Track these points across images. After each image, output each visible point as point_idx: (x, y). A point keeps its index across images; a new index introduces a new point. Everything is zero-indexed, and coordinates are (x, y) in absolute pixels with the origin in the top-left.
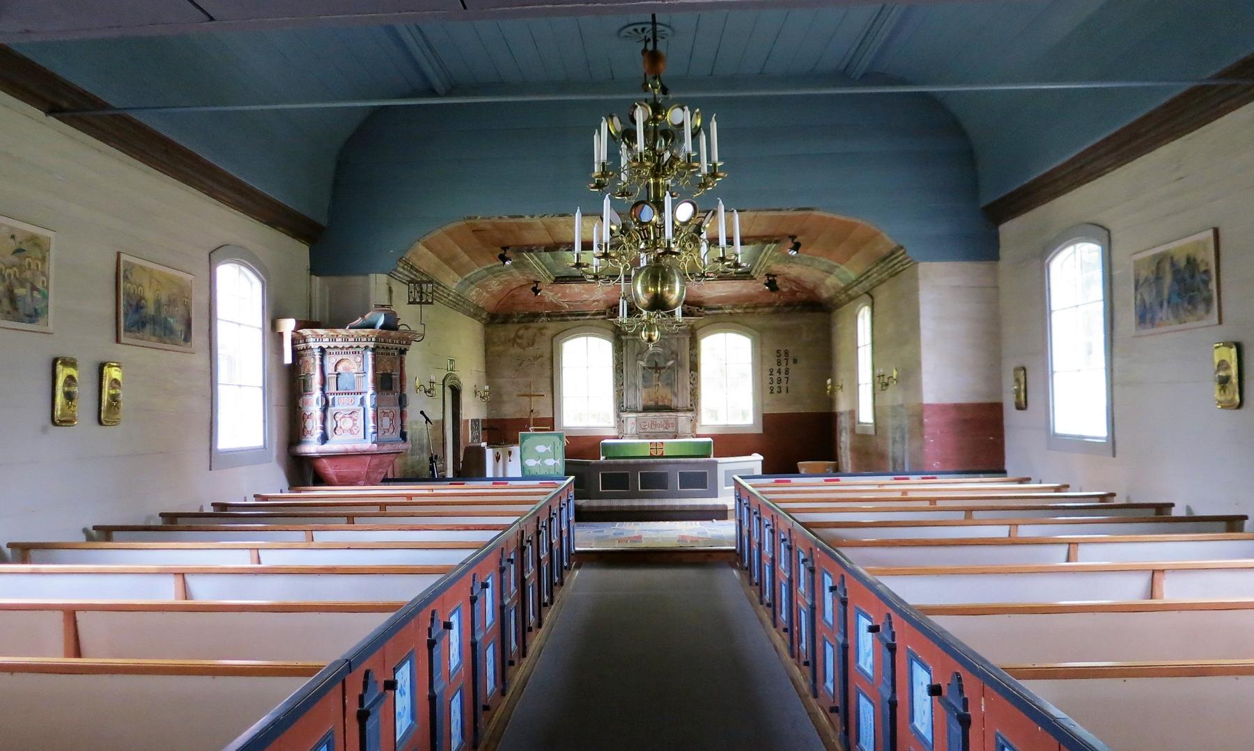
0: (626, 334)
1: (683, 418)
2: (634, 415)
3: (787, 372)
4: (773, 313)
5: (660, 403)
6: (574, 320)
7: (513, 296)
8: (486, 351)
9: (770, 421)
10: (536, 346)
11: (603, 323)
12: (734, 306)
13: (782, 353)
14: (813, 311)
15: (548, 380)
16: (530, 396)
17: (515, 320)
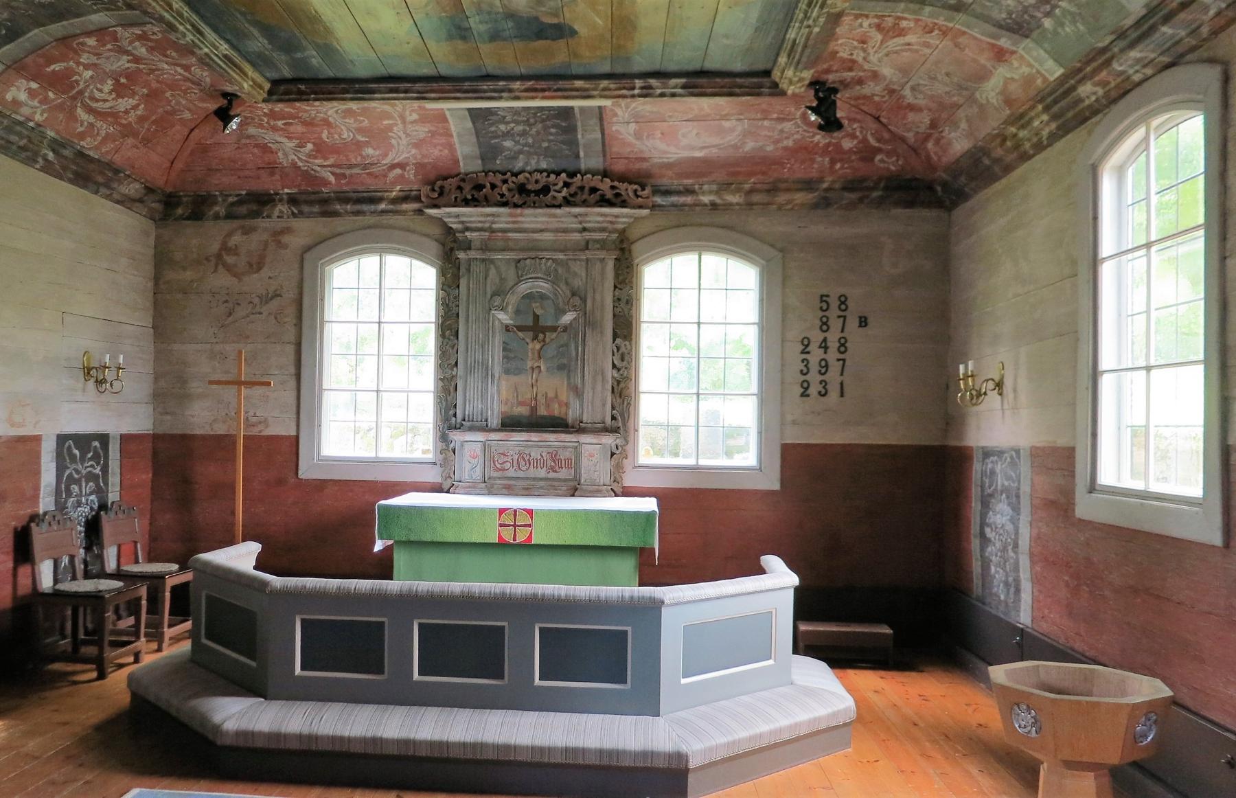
0: (467, 246)
1: (593, 448)
2: (480, 436)
3: (843, 346)
4: (815, 206)
5: (542, 411)
6: (350, 209)
7: (204, 149)
8: (157, 279)
9: (800, 462)
10: (265, 272)
11: (418, 223)
12: (725, 187)
13: (834, 303)
14: (910, 204)
15: (290, 349)
16: (239, 383)
17: (220, 209)
